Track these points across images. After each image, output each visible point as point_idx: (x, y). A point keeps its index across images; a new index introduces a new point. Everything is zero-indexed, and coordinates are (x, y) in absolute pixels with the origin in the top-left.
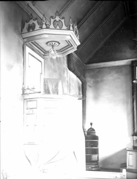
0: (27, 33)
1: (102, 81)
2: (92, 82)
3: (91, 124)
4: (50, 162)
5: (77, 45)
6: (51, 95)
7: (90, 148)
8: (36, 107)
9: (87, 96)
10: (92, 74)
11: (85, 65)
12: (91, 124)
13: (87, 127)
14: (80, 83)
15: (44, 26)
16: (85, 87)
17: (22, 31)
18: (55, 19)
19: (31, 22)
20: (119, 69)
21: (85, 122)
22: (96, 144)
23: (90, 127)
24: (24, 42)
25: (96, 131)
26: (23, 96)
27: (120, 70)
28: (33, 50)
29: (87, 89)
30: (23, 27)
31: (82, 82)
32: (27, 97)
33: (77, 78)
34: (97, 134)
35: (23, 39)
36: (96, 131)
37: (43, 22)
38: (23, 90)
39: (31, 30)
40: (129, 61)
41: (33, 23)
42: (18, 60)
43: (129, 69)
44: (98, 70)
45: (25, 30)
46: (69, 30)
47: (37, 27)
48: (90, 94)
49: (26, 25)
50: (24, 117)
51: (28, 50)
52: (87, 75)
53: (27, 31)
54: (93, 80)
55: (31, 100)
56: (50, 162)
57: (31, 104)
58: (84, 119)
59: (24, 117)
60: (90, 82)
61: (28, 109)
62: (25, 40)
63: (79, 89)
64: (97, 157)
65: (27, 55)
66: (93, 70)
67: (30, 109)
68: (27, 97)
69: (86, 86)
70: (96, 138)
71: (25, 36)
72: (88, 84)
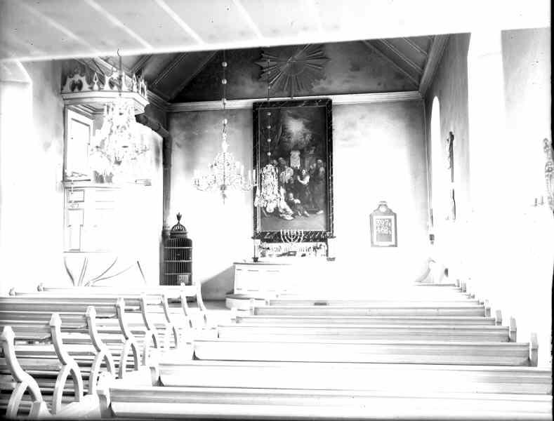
0: (68, 93)
1: (201, 136)
2: (182, 138)
3: (179, 217)
4: (102, 277)
5: (143, 105)
6: (106, 184)
7: (176, 261)
8: (82, 200)
9: (172, 163)
10: (183, 121)
11: (169, 104)
12: (179, 217)
13: (172, 222)
14: (160, 139)
15: (96, 87)
16: (168, 147)
17: (62, 89)
18: (112, 76)
19: (77, 78)
20: (231, 115)
21: (168, 213)
22: (186, 254)
23: (176, 222)
24: (65, 105)
25: (543, 169)
26: (64, 184)
27: (234, 116)
28: (78, 112)
29: (173, 149)
30: (64, 83)
31: (164, 139)
32: (68, 185)
33: (153, 131)
34: (189, 236)
35: (64, 99)
36: (187, 231)
37: (94, 81)
38: (65, 179)
39: (76, 90)
40: (248, 103)
41: (80, 81)
42: (57, 134)
43: (250, 116)
44: (194, 114)
45: (67, 88)
46: (132, 91)
47: (86, 86)
48: (178, 159)
49: (69, 81)
50: (276, 389)
51: (71, 114)
52: (175, 122)
53: (69, 90)
54: (184, 133)
55: (77, 189)
56: (102, 277)
57: (76, 196)
58: (166, 208)
59: (276, 389)
60: (178, 136)
61: (70, 202)
62: (67, 102)
63: (157, 152)
64: (187, 278)
65: (70, 123)
66: (183, 113)
67: (76, 202)
68: (68, 185)
69: (171, 146)
70: (187, 243)
71: (66, 96)
72: (175, 140)
